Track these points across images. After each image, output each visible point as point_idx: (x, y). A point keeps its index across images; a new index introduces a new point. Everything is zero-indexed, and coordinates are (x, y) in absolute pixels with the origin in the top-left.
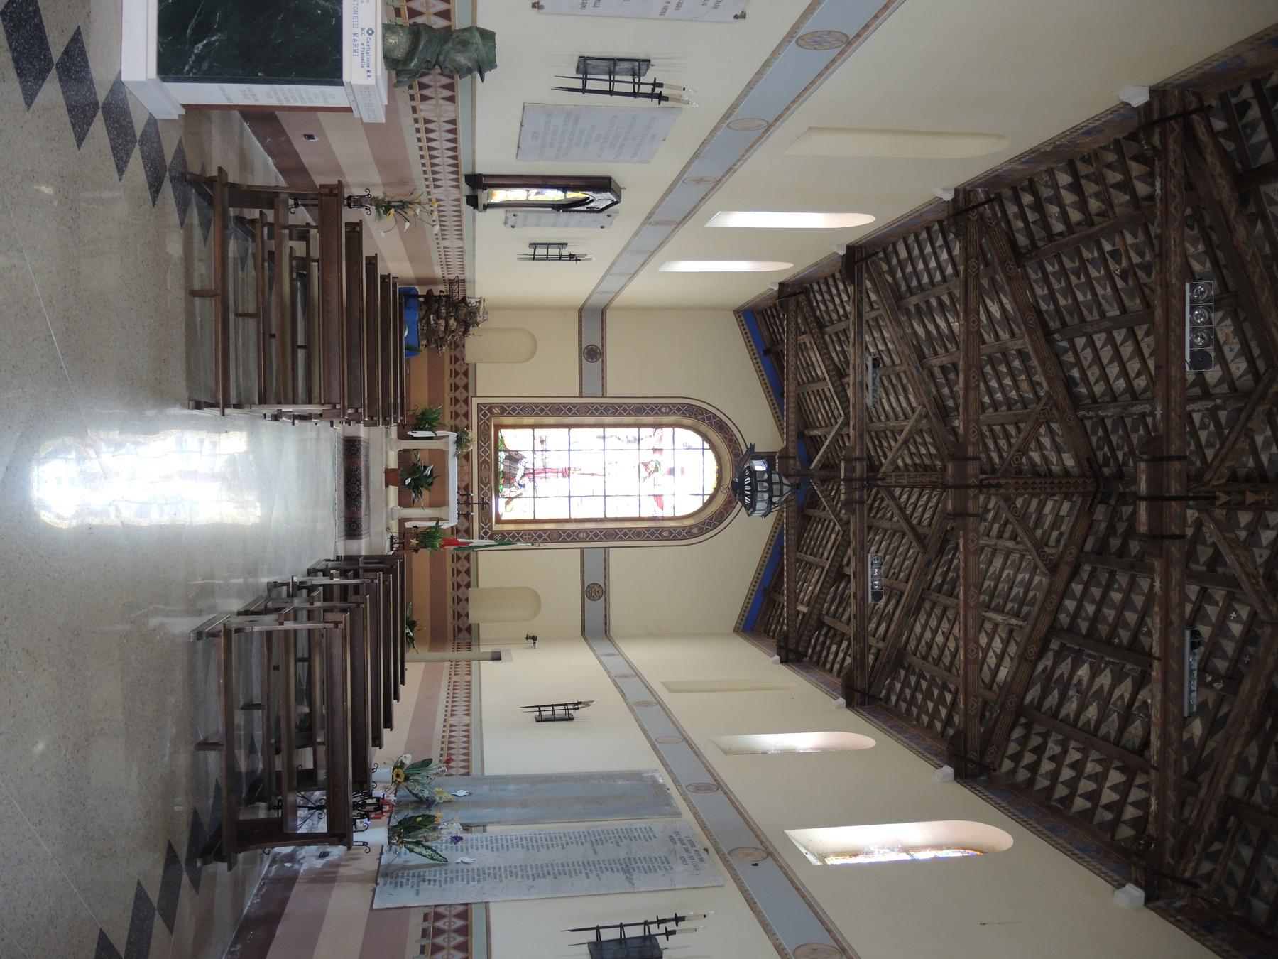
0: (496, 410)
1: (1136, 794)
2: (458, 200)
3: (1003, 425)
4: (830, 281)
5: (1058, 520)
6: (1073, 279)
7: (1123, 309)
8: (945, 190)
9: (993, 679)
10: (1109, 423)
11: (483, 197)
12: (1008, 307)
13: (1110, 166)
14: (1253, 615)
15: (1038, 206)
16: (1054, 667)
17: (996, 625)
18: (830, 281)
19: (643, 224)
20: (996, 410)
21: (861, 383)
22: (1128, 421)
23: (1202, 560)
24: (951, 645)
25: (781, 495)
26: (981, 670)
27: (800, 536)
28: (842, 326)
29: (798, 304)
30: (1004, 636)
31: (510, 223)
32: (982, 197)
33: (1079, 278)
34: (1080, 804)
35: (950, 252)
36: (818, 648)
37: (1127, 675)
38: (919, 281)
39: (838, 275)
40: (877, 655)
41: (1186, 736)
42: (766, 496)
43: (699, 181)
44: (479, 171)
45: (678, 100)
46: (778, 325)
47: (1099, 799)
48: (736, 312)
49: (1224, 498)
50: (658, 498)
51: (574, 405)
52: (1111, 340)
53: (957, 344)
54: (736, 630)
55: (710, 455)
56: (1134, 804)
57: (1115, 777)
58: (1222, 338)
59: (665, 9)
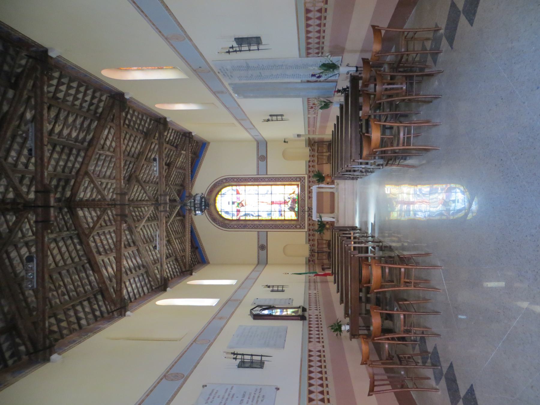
0: (298, 226)
1: (52, 89)
2: (310, 310)
3: (107, 225)
4: (173, 276)
5: (85, 191)
6: (79, 283)
7: (60, 273)
8: (129, 316)
9: (109, 130)
10: (65, 229)
11: (300, 312)
12: (105, 271)
13: (65, 328)
14: (6, 159)
15: (93, 311)
16: (86, 136)
17: (109, 150)
18: (173, 276)
19: (242, 300)
20: (109, 231)
21: (161, 240)
22: (58, 230)
23: (27, 179)
24: (126, 142)
25: (191, 202)
26: (114, 133)
27: (184, 179)
28: (168, 260)
29: (185, 268)
30: (106, 146)
31: (291, 300)
32: (115, 313)
33: (78, 284)
34: (75, 85)
35: (127, 291)
36: (177, 138)
37: (57, 134)
38: (139, 279)
39: (170, 279)
40: (155, 136)
41: (33, 112)
42: (196, 202)
43: (221, 318)
44: (302, 322)
45: (227, 353)
46: (192, 259)
47: (67, 87)
48: (209, 263)
49: (20, 206)
50: (238, 193)
51: (269, 228)
52: (64, 261)
53: (124, 255)
54: (209, 143)
55: (219, 209)
56: (53, 85)
57: (61, 95)
58: (21, 265)
59: (232, 387)
